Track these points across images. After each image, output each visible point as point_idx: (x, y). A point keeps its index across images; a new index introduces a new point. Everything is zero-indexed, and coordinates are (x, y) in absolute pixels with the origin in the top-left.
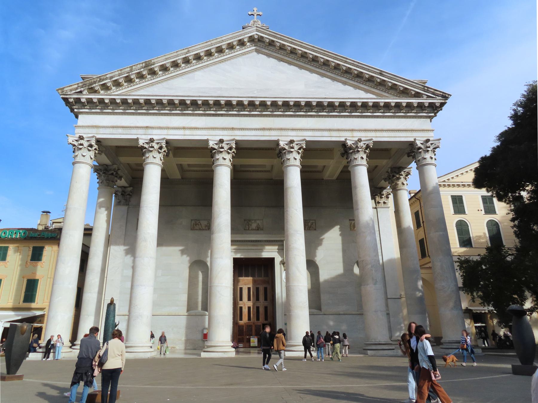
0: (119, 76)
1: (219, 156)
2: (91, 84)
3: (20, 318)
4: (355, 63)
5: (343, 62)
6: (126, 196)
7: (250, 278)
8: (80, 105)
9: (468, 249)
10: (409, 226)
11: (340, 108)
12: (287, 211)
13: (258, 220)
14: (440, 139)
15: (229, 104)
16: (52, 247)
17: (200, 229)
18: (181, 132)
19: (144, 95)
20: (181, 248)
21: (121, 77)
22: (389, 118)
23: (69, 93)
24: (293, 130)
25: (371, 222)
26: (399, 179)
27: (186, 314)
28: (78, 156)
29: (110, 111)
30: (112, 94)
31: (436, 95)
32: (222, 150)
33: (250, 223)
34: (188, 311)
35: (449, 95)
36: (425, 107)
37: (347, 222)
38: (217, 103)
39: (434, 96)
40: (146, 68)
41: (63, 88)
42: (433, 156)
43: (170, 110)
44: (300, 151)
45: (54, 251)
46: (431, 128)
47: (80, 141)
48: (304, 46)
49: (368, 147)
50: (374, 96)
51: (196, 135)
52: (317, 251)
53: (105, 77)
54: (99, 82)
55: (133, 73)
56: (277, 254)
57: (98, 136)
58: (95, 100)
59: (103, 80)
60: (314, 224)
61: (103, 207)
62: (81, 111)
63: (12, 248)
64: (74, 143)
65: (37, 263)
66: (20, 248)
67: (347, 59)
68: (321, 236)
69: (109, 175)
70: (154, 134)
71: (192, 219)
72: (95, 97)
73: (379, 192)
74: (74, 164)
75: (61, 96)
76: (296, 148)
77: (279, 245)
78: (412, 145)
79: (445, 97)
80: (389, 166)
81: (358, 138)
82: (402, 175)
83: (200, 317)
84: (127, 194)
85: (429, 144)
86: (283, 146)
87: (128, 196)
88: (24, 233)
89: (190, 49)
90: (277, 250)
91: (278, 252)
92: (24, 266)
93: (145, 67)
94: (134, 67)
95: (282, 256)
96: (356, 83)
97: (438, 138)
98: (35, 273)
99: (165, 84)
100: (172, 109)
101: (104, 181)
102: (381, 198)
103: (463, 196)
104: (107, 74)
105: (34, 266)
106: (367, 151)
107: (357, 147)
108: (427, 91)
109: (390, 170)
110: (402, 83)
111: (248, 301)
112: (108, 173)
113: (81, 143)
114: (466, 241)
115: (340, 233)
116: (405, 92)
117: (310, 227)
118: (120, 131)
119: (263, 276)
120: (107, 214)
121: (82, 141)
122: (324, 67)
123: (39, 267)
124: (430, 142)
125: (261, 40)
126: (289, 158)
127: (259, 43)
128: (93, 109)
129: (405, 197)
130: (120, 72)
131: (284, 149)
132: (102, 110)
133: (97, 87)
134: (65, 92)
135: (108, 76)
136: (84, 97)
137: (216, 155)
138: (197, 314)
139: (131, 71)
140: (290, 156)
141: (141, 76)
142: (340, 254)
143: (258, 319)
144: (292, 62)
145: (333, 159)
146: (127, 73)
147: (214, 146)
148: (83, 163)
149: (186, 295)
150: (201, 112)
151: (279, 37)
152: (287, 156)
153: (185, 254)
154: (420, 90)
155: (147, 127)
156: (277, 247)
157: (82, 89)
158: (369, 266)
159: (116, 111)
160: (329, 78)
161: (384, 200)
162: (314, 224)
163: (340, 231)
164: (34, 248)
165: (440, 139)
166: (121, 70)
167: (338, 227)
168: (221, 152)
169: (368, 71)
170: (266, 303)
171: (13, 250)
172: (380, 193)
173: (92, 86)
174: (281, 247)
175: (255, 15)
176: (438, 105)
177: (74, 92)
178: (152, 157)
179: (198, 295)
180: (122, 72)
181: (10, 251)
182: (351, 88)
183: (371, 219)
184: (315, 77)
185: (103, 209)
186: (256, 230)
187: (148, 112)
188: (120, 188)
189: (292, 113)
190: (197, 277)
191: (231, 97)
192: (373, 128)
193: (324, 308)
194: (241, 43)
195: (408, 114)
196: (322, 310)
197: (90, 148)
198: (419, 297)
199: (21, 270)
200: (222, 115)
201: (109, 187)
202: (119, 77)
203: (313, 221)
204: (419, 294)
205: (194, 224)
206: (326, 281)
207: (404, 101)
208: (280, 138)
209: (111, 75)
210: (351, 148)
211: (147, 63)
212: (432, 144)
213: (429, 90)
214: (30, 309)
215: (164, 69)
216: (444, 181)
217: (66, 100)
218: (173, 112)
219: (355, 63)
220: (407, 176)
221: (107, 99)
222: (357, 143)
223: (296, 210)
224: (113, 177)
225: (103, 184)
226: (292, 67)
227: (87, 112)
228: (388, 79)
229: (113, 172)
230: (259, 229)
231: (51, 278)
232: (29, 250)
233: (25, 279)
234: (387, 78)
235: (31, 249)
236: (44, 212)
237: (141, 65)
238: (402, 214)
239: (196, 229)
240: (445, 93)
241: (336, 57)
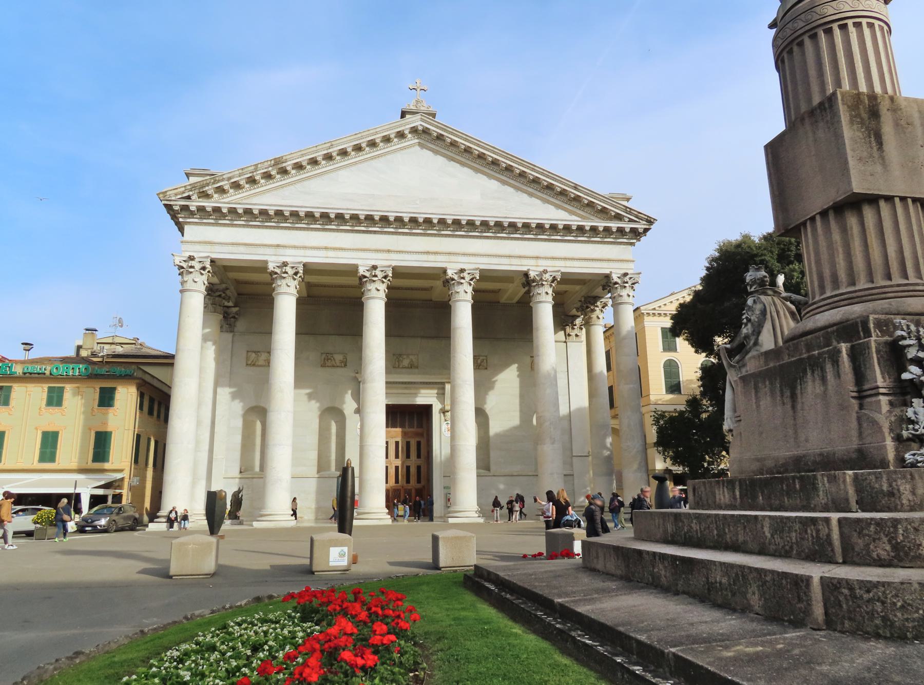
1: (371, 287)
2: (203, 187)
3: (102, 483)
4: (545, 172)
7: (399, 430)
8: (187, 213)
9: (676, 396)
10: (602, 371)
12: (454, 356)
13: (412, 355)
14: (640, 273)
16: (128, 389)
17: (333, 366)
18: (322, 253)
20: (308, 391)
21: (242, 177)
23: (173, 198)
24: (464, 254)
25: (553, 372)
26: (593, 311)
27: (317, 476)
28: (188, 282)
29: (228, 222)
32: (375, 279)
33: (401, 359)
34: (318, 472)
35: (655, 219)
36: (626, 232)
37: (528, 360)
38: (369, 218)
39: (638, 220)
40: (274, 167)
41: (166, 192)
42: (631, 294)
44: (472, 282)
46: (632, 259)
47: (191, 262)
49: (554, 279)
52: (487, 396)
53: (221, 178)
54: (214, 183)
55: (258, 172)
56: (435, 399)
57: (214, 256)
58: (209, 209)
59: (219, 181)
60: (485, 361)
61: (210, 340)
63: (69, 388)
64: (181, 264)
65: (107, 410)
66: (81, 390)
67: (535, 166)
68: (493, 378)
69: (216, 296)
70: (287, 254)
71: (323, 352)
72: (208, 204)
73: (570, 321)
74: (182, 291)
75: (163, 202)
76: (468, 278)
77: (438, 389)
79: (650, 221)
80: (583, 294)
82: (597, 306)
84: (231, 316)
85: (626, 279)
86: (451, 276)
87: (232, 319)
88: (85, 369)
89: (333, 143)
91: (437, 398)
92: (89, 415)
93: (274, 165)
94: (259, 166)
95: (442, 402)
96: (545, 196)
97: (639, 272)
98: (105, 424)
99: (298, 186)
100: (310, 222)
101: (210, 305)
102: (573, 329)
105: (104, 414)
106: (553, 285)
107: (541, 279)
108: (630, 213)
109: (583, 299)
110: (600, 201)
111: (409, 466)
112: (215, 295)
113: (192, 265)
114: (674, 387)
115: (517, 373)
117: (480, 366)
119: (415, 427)
120: (214, 350)
121: (193, 262)
122: (506, 173)
123: (111, 415)
124: (628, 276)
125: (426, 131)
126: (458, 291)
127: (424, 136)
129: (598, 332)
130: (241, 171)
131: (453, 279)
133: (210, 190)
135: (224, 177)
136: (193, 205)
137: (368, 284)
138: (331, 476)
139: (256, 170)
140: (460, 289)
141: (268, 176)
142: (517, 401)
143: (408, 481)
145: (513, 283)
146: (250, 173)
147: (365, 274)
148: (195, 291)
149: (316, 452)
150: (348, 228)
152: (456, 287)
153: (314, 399)
155: (278, 246)
156: (436, 391)
157: (191, 193)
158: (547, 424)
159: (235, 222)
160: (512, 187)
161: (576, 331)
162: (485, 361)
163: (518, 371)
165: (640, 273)
166: (242, 169)
167: (516, 365)
168: (374, 281)
169: (560, 183)
170: (419, 462)
171: (70, 392)
172: (572, 323)
173: (204, 190)
174: (441, 391)
175: (418, 90)
176: (641, 231)
178: (285, 285)
179: (330, 452)
180: (244, 171)
183: (553, 368)
185: (210, 344)
186: (408, 368)
190: (329, 429)
191: (388, 212)
192: (563, 255)
193: (493, 467)
194: (401, 135)
195: (606, 240)
196: (491, 470)
197: (202, 271)
198: (606, 456)
199: (86, 420)
200: (375, 232)
201: (216, 314)
202: (240, 178)
203: (485, 358)
204: (606, 453)
205: (325, 359)
206: (497, 435)
207: (601, 224)
209: (229, 175)
210: (534, 281)
211: (277, 160)
212: (631, 278)
213: (632, 211)
214: (103, 471)
215: (299, 167)
216: (654, 309)
217: (169, 208)
218: (312, 226)
219: (545, 172)
220: (603, 307)
221: (225, 207)
222: (542, 275)
223: (465, 356)
224: (220, 299)
226: (466, 170)
227: (196, 222)
228: (585, 194)
229: (221, 293)
230: (412, 366)
233: (39, 431)
236: (87, 330)
237: (269, 163)
238: (594, 356)
239: (328, 366)
240: (650, 217)
241: (522, 162)
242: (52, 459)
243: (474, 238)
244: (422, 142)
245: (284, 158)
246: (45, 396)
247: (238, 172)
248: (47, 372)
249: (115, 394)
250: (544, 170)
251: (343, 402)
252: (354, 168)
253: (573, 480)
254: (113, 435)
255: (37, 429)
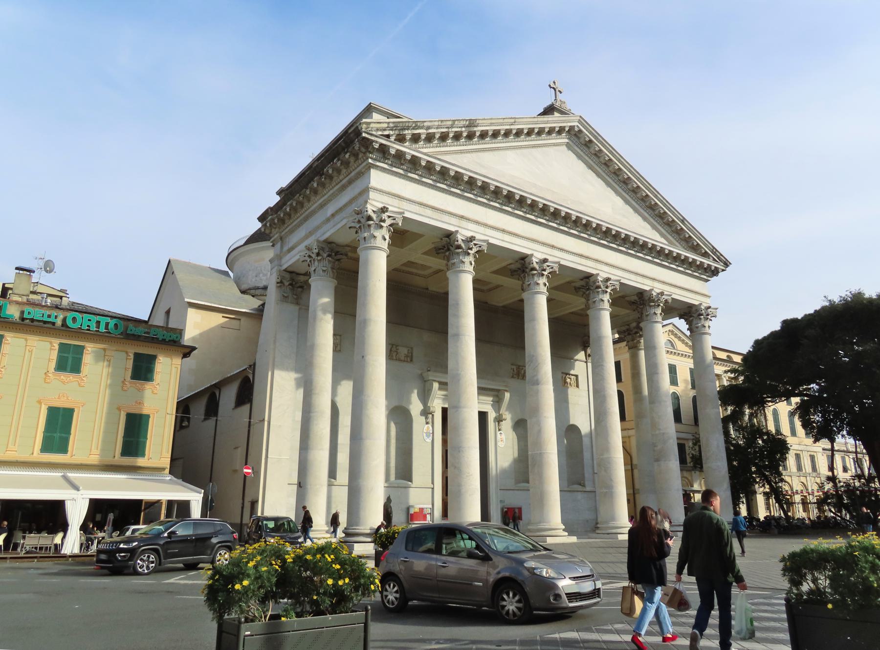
0: (437, 128)
2: (403, 129)
4: (664, 201)
5: (653, 195)
6: (295, 289)
11: (409, 165)
14: (717, 309)
15: (567, 218)
19: (471, 171)
22: (517, 217)
23: (374, 133)
24: (607, 264)
30: (419, 150)
31: (720, 260)
43: (488, 200)
45: (176, 366)
48: (622, 161)
50: (667, 243)
51: (515, 244)
62: (378, 164)
63: (91, 349)
77: (494, 396)
78: (524, 259)
79: (727, 264)
81: (661, 291)
83: (403, 489)
84: (298, 285)
89: (517, 120)
90: (492, 403)
91: (492, 405)
93: (467, 126)
94: (456, 123)
97: (717, 307)
98: (140, 403)
100: (491, 199)
101: (330, 269)
103: (677, 366)
104: (425, 121)
105: (139, 390)
108: (714, 254)
110: (697, 238)
116: (695, 248)
118: (429, 212)
124: (547, 264)
128: (395, 167)
130: (440, 123)
132: (407, 172)
134: (370, 129)
139: (452, 127)
144: (602, 175)
146: (446, 128)
151: (600, 140)
154: (709, 250)
155: (462, 217)
156: (491, 399)
157: (391, 133)
159: (424, 180)
164: (137, 356)
166: (442, 121)
173: (404, 133)
174: (496, 399)
177: (380, 133)
181: (87, 355)
182: (648, 226)
184: (619, 201)
187: (435, 184)
188: (288, 273)
189: (417, 176)
199: (113, 396)
200: (540, 224)
207: (691, 256)
208: (460, 230)
211: (472, 122)
213: (717, 253)
225: (327, 274)
231: (172, 414)
232: (51, 349)
233: (122, 412)
234: (686, 227)
235: (132, 356)
240: (728, 261)
242: (63, 448)
243: (611, 250)
244: (571, 143)
245: (477, 121)
246: (54, 355)
247: (436, 123)
248: (59, 322)
249: (155, 364)
250: (664, 199)
251: (409, 402)
252: (519, 151)
253: (595, 496)
254: (151, 420)
255: (40, 402)
